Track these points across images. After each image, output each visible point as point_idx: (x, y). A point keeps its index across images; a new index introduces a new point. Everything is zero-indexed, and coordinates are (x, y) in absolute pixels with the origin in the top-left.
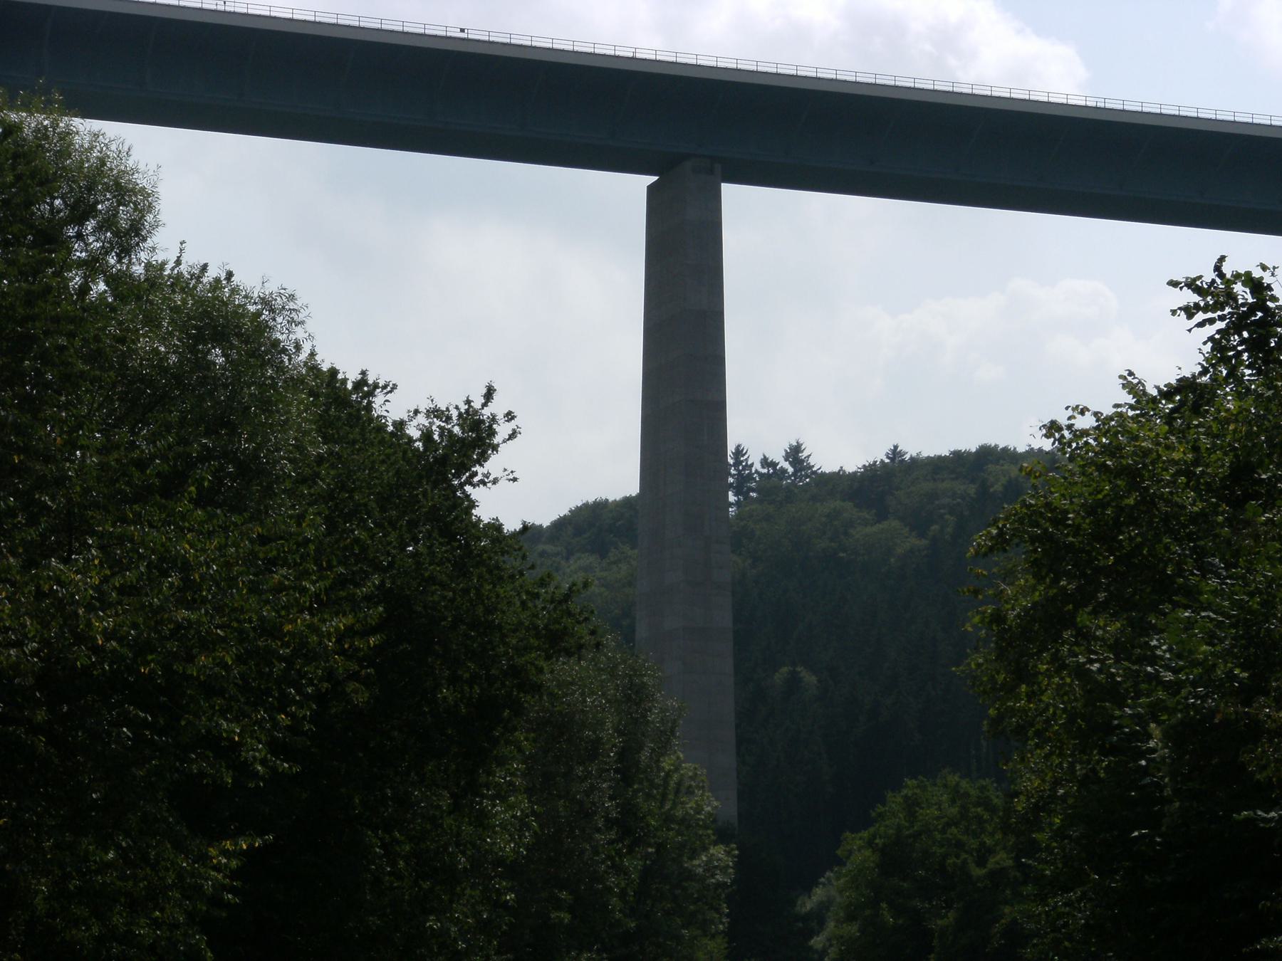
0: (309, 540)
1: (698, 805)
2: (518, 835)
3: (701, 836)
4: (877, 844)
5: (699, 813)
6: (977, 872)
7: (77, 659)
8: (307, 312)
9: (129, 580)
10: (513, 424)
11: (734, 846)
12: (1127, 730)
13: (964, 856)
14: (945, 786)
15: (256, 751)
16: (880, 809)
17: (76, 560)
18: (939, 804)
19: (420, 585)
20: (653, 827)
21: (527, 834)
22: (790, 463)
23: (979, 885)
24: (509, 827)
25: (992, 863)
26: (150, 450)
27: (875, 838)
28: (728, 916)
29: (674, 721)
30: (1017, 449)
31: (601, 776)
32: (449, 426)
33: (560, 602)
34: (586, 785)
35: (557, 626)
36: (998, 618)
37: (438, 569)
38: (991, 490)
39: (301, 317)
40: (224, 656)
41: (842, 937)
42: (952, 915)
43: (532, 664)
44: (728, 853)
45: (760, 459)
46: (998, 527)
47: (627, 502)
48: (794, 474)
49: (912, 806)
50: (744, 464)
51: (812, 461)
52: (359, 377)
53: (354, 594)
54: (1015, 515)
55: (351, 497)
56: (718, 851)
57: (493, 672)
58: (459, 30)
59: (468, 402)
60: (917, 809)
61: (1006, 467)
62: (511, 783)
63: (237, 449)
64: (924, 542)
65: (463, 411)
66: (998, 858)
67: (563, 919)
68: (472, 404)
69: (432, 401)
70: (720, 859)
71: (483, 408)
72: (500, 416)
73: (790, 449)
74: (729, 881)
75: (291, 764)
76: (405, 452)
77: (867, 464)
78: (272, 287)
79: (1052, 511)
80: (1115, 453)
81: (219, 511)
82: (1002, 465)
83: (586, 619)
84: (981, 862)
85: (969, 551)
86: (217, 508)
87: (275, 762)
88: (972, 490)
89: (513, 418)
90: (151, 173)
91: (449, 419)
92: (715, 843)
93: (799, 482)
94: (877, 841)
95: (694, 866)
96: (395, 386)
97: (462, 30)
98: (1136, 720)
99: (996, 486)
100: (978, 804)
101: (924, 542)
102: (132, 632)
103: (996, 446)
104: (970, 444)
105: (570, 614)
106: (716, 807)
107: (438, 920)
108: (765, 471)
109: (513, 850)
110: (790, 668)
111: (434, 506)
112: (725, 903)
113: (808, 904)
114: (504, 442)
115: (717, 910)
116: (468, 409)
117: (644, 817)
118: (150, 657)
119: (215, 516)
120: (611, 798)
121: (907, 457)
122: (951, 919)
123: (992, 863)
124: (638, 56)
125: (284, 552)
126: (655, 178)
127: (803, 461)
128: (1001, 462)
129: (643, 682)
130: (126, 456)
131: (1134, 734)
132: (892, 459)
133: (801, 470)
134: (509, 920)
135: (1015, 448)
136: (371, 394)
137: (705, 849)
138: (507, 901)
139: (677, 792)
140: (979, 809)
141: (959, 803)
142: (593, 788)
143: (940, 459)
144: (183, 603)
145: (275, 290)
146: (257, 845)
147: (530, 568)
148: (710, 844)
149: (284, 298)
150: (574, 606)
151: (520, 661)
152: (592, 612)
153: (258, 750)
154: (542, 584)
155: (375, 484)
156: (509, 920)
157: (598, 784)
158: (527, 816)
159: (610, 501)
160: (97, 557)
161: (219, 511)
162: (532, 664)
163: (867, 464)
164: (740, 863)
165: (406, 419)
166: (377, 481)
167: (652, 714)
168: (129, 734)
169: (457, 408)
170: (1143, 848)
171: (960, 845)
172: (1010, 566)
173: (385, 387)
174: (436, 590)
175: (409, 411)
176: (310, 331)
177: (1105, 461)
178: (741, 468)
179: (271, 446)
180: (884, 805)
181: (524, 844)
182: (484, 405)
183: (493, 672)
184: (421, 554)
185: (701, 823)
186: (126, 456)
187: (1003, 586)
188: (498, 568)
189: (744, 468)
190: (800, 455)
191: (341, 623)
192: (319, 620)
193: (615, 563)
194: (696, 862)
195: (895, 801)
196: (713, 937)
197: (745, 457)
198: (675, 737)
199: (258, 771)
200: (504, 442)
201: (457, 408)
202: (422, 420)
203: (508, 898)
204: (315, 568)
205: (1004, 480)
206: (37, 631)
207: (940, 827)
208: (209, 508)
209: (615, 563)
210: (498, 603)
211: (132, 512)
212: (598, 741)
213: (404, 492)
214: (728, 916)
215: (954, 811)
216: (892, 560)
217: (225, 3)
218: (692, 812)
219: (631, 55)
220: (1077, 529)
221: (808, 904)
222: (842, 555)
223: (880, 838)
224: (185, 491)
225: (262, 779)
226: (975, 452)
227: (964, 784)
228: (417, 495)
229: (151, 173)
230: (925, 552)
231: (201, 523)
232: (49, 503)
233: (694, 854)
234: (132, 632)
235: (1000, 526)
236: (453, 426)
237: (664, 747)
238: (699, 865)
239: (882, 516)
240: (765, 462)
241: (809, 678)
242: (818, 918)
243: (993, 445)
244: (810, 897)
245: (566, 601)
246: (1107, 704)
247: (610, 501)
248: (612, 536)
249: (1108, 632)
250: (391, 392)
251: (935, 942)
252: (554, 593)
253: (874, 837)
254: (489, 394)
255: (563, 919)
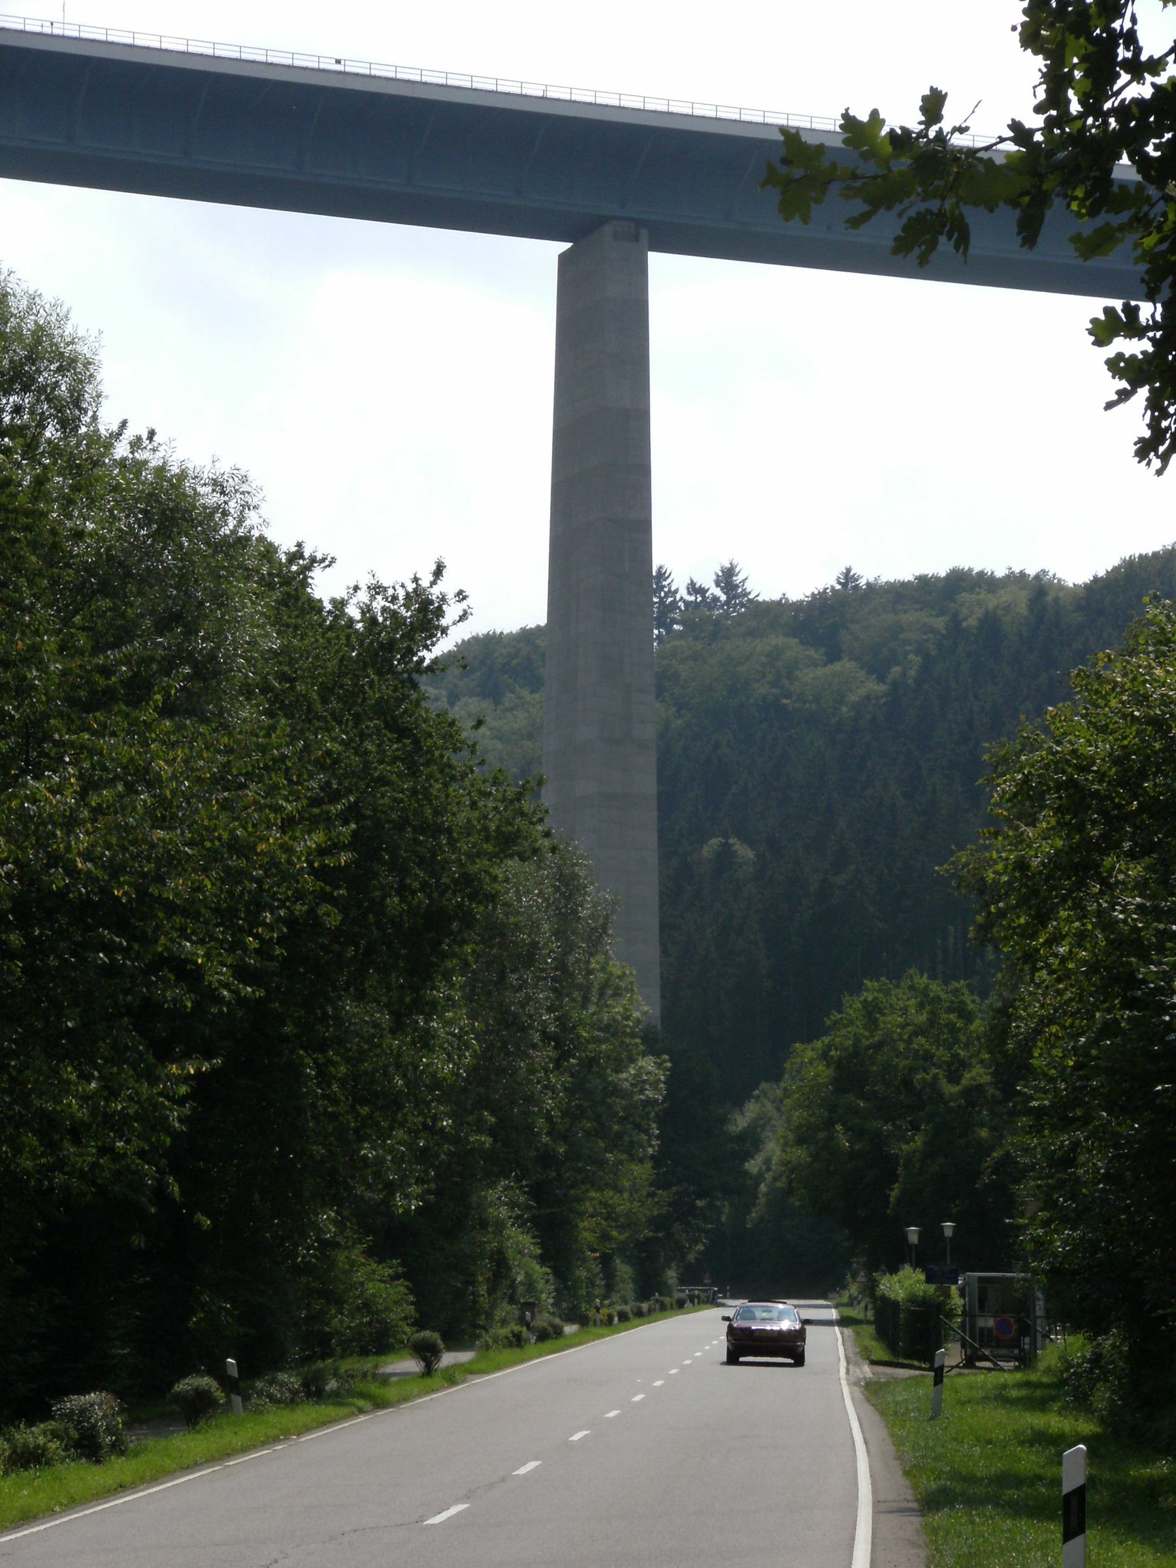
0: (287, 756)
1: (626, 1010)
2: (458, 1055)
3: (628, 1045)
4: (832, 1057)
5: (627, 1018)
6: (950, 1089)
7: (53, 882)
8: (260, 496)
9: (105, 799)
10: (464, 605)
11: (666, 1057)
12: (1152, 985)
13: (934, 1071)
14: (911, 988)
15: (219, 974)
16: (836, 1016)
17: (49, 777)
18: (905, 1009)
19: (368, 786)
20: (585, 1038)
21: (467, 1054)
22: (722, 589)
23: (952, 1104)
24: (446, 1045)
25: (967, 1078)
26: (115, 656)
27: (830, 1050)
28: (658, 1137)
29: (607, 917)
30: (995, 574)
31: (537, 985)
32: (396, 607)
33: (512, 801)
34: (521, 995)
35: (510, 828)
36: (1022, 865)
37: (388, 768)
38: (964, 624)
39: (255, 501)
40: (203, 880)
41: (789, 1162)
42: (919, 1140)
43: (486, 872)
44: (659, 1065)
45: (686, 584)
46: (1023, 774)
47: (526, 636)
48: (727, 602)
49: (872, 1012)
50: (666, 589)
51: (748, 586)
52: (294, 549)
53: (328, 812)
54: (1040, 761)
55: (292, 688)
56: (648, 1063)
57: (443, 880)
58: (334, 61)
59: (416, 580)
60: (878, 1016)
61: (982, 596)
62: (449, 998)
63: (195, 648)
64: (882, 688)
65: (411, 590)
66: (974, 1073)
67: (484, 1143)
68: (420, 582)
69: (374, 576)
70: (650, 1073)
71: (431, 587)
72: (450, 596)
73: (722, 571)
74: (661, 1098)
75: (254, 988)
76: (348, 637)
77: (816, 592)
78: (224, 467)
79: (1078, 757)
80: (1142, 702)
81: (188, 722)
82: (978, 593)
83: (541, 820)
84: (954, 1078)
85: (993, 797)
86: (186, 719)
87: (237, 985)
88: (940, 623)
89: (464, 598)
90: (92, 339)
91: (394, 598)
92: (644, 1054)
93: (734, 612)
94: (832, 1053)
95: (620, 1080)
96: (333, 560)
97: (338, 62)
98: (1161, 975)
99: (970, 620)
100: (949, 1010)
101: (882, 688)
102: (107, 853)
103: (970, 570)
104: (941, 569)
105: (522, 814)
106: (646, 1013)
107: (372, 1148)
108: (692, 598)
109: (452, 1072)
110: (720, 839)
111: (382, 698)
112: (654, 1122)
113: (740, 1122)
114: (454, 624)
115: (646, 1132)
116: (417, 588)
117: (574, 1027)
118: (122, 879)
119: (185, 727)
120: (550, 1010)
121: (862, 582)
122: (919, 1143)
123: (967, 1078)
124: (550, 95)
125: (259, 768)
126: (569, 245)
127: (737, 586)
128: (977, 590)
129: (573, 873)
130: (90, 662)
131: (1159, 990)
132: (844, 585)
133: (736, 597)
134: (448, 1149)
135: (993, 573)
136: (308, 568)
137: (632, 1060)
138: (443, 1128)
139: (601, 994)
140: (951, 1016)
141: (928, 1008)
142: (529, 998)
143: (904, 585)
144: (159, 823)
145: (228, 470)
146: (204, 1069)
147: (479, 764)
148: (638, 1054)
149: (236, 479)
150: (527, 805)
151: (473, 869)
152: (547, 812)
153: (221, 974)
154: (495, 782)
155: (319, 674)
156: (448, 1149)
157: (534, 994)
158: (467, 1033)
159: (505, 633)
160: (74, 775)
161: (188, 722)
162: (486, 872)
163: (816, 592)
164: (673, 1081)
165: (346, 598)
166: (320, 670)
167: (583, 910)
168: (106, 960)
169: (403, 586)
170: (1166, 1101)
171: (927, 1057)
172: (1002, 753)
173: (323, 560)
174: (386, 791)
175: (348, 588)
176: (264, 516)
177: (1133, 711)
178: (662, 594)
179: (230, 644)
180: (840, 1012)
181: (463, 1065)
182: (433, 583)
183: (443, 880)
184: (371, 752)
185: (628, 1030)
186: (90, 662)
187: (1023, 828)
188: (450, 766)
189: (667, 595)
190: (734, 578)
191: (316, 839)
192: (290, 838)
193: (511, 709)
194: (624, 1075)
195: (853, 1006)
196: (641, 1161)
197: (668, 581)
198: (608, 935)
199: (224, 997)
200: (454, 624)
201: (403, 586)
202: (363, 596)
203: (445, 1123)
204: (285, 782)
205: (979, 612)
206: (10, 851)
207: (906, 1037)
208: (177, 718)
209: (511, 709)
210: (449, 804)
211: (96, 721)
212: (534, 944)
213: (348, 681)
214: (658, 1137)
215: (923, 1018)
216: (844, 709)
217: (52, 24)
218: (619, 1018)
219: (540, 94)
220: (1101, 776)
221: (740, 1122)
222: (785, 701)
223: (836, 1049)
224: (151, 699)
225: (228, 1004)
226: (944, 578)
227: (936, 988)
228: (363, 686)
229: (92, 339)
230: (884, 700)
231: (168, 733)
232: (13, 712)
233: (619, 1068)
234: (107, 853)
235: (1026, 772)
236: (399, 608)
237: (595, 943)
238: (626, 1080)
239: (833, 656)
240: (693, 588)
241: (744, 852)
242: (750, 1141)
243: (966, 569)
244: (742, 1113)
245: (519, 800)
246: (1133, 959)
247: (505, 633)
248: (506, 676)
249: (1129, 876)
250: (329, 566)
251: (900, 1170)
252: (505, 791)
253: (829, 1047)
254: (438, 572)
255: (484, 1143)
